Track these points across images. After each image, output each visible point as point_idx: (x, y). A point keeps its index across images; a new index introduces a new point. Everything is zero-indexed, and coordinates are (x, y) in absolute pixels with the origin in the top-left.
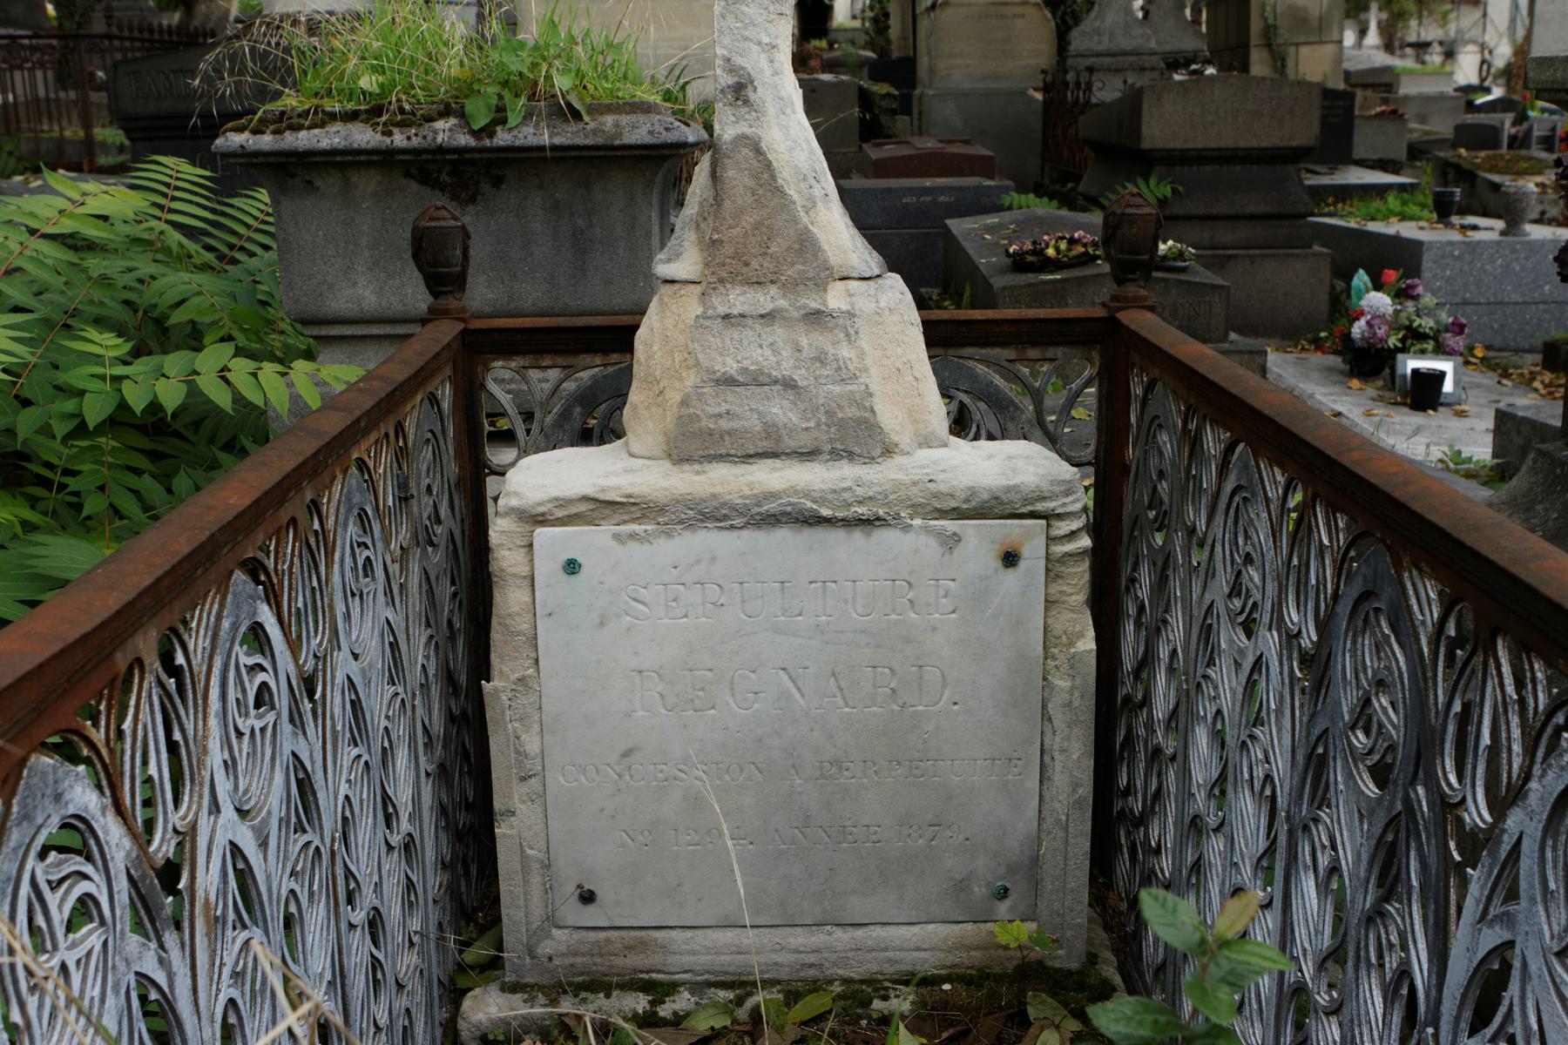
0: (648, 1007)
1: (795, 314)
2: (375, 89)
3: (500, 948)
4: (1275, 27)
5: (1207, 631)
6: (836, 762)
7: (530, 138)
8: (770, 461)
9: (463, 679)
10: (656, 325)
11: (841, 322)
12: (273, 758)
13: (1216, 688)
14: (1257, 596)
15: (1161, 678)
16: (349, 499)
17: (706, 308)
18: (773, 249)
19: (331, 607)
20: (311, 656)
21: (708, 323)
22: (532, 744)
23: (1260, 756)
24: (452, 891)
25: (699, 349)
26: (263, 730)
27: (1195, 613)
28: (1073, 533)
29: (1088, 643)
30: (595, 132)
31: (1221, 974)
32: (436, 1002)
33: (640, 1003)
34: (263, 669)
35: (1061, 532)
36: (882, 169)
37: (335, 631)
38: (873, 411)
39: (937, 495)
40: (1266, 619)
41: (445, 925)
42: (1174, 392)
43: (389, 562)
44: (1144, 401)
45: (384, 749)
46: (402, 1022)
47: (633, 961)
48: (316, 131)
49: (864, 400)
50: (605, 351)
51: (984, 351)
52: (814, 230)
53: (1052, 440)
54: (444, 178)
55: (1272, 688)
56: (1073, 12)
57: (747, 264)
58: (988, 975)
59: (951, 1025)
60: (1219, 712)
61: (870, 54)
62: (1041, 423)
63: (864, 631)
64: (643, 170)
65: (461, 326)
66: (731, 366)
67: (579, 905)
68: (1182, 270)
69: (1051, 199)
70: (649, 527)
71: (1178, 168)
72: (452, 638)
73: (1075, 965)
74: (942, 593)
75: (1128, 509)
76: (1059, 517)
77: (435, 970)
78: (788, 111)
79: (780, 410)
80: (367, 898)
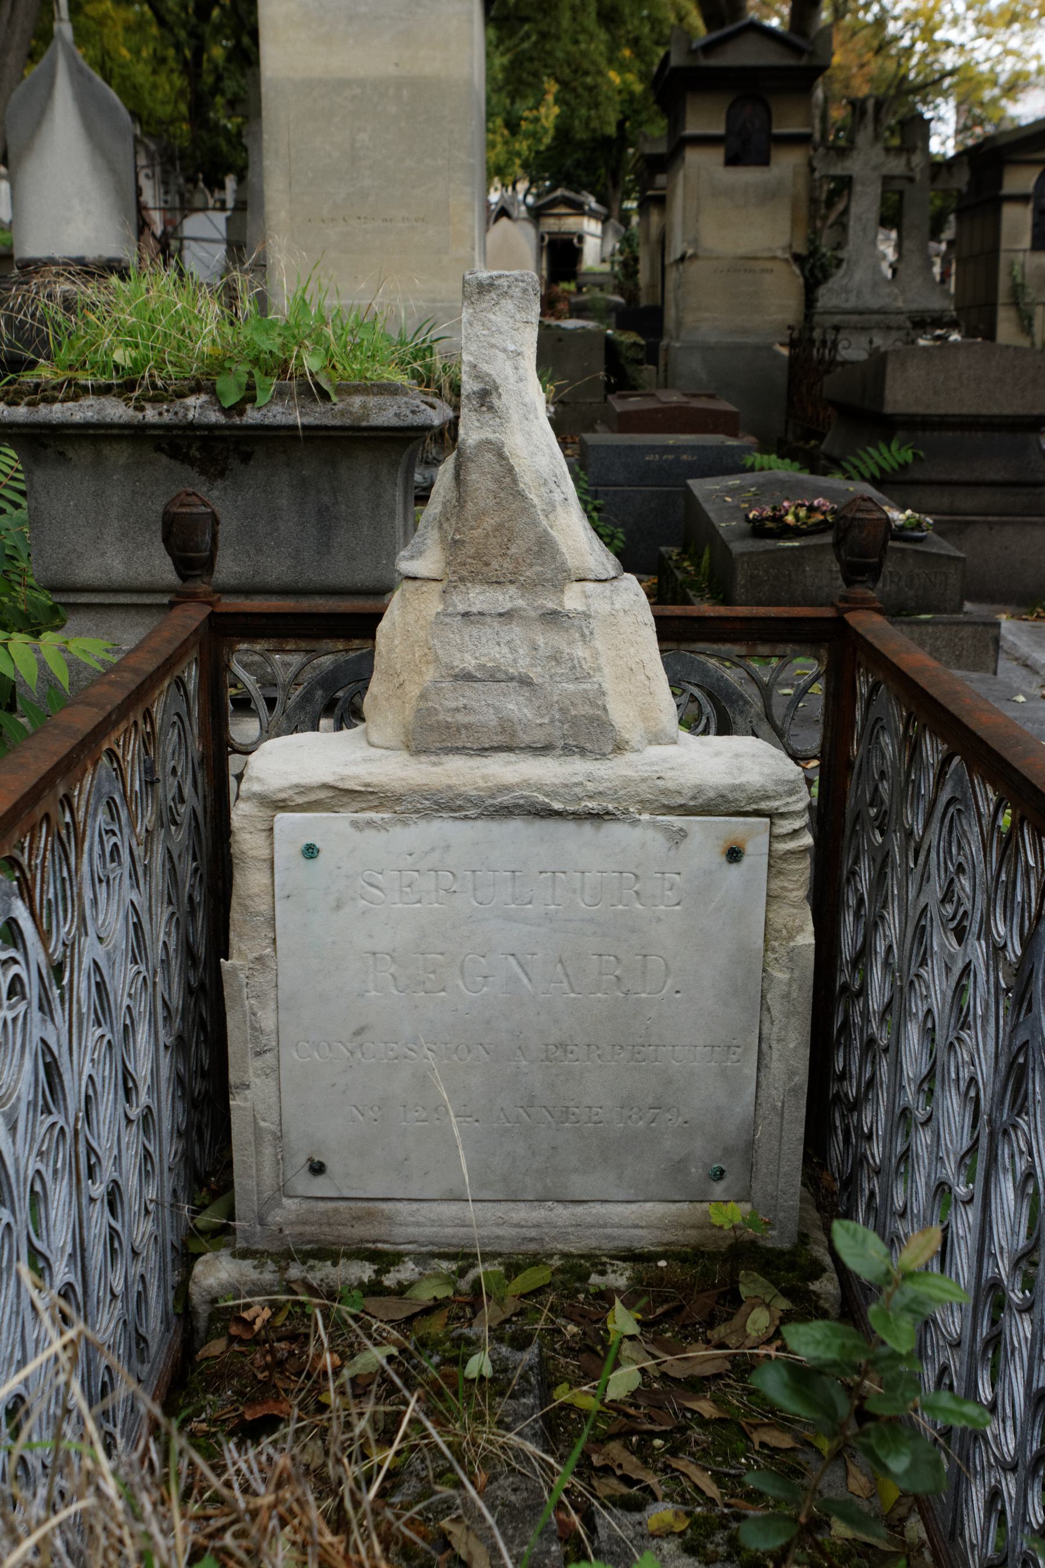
0: (373, 1277)
1: (533, 614)
2: (129, 364)
3: (231, 1216)
4: (1023, 286)
5: (921, 932)
6: (561, 1046)
7: (279, 417)
8: (504, 755)
9: (202, 951)
10: (398, 619)
11: (576, 622)
12: (23, 1046)
13: (928, 988)
14: (967, 905)
15: (877, 972)
16: (99, 790)
17: (447, 606)
18: (513, 550)
19: (80, 896)
20: (60, 945)
21: (447, 620)
22: (267, 1020)
23: (967, 1058)
24: (187, 1158)
25: (438, 645)
26: (15, 1020)
27: (911, 913)
28: (795, 831)
29: (807, 938)
30: (342, 413)
31: (905, 1300)
32: (170, 1265)
33: (365, 1272)
34: (15, 961)
35: (784, 831)
36: (627, 423)
37: (83, 919)
38: (605, 709)
39: (665, 792)
40: (975, 928)
41: (180, 1192)
42: (897, 698)
43: (134, 847)
44: (869, 702)
45: (126, 1026)
46: (137, 1287)
47: (360, 1231)
48: (70, 404)
49: (597, 698)
50: (348, 637)
51: (715, 647)
52: (553, 533)
53: (780, 736)
54: (194, 452)
55: (979, 997)
56: (822, 266)
57: (487, 564)
58: (702, 1252)
59: (666, 1301)
60: (929, 1011)
61: (618, 299)
62: (769, 717)
63: (591, 920)
64: (390, 452)
65: (208, 610)
66: (469, 662)
67: (309, 1175)
68: (920, 540)
69: (793, 460)
70: (386, 816)
71: (920, 433)
72: (192, 913)
73: (786, 1246)
74: (667, 885)
75: (851, 802)
76: (783, 815)
77: (169, 1237)
78: (531, 416)
79: (516, 706)
80: (107, 1171)
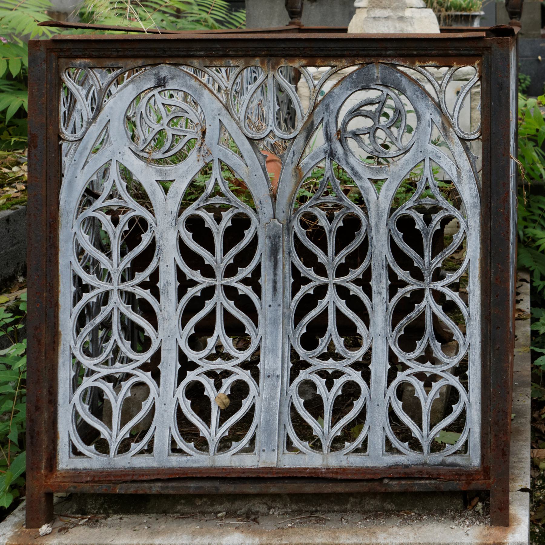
11: (409, 20)
21: (368, 19)
57: (381, 2)
